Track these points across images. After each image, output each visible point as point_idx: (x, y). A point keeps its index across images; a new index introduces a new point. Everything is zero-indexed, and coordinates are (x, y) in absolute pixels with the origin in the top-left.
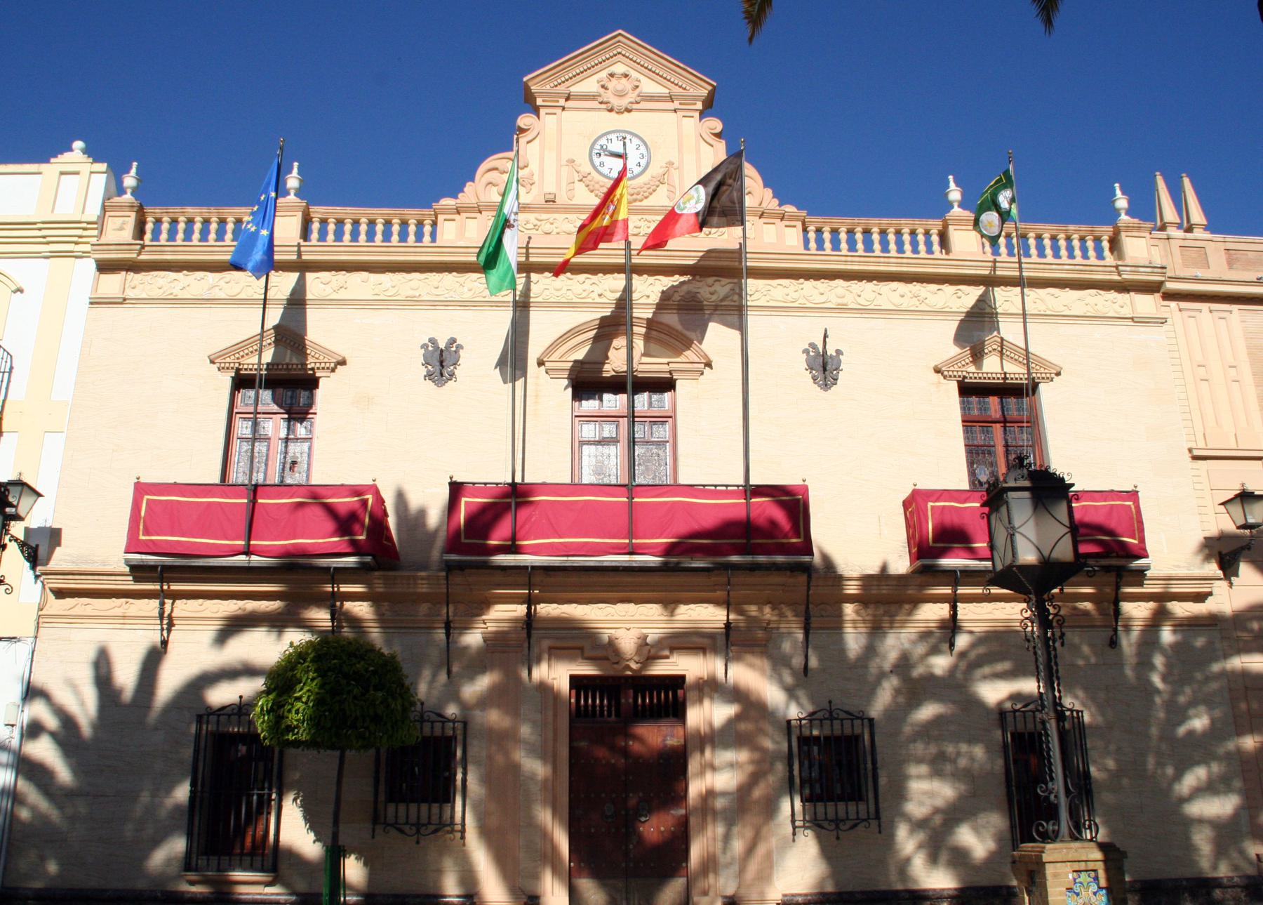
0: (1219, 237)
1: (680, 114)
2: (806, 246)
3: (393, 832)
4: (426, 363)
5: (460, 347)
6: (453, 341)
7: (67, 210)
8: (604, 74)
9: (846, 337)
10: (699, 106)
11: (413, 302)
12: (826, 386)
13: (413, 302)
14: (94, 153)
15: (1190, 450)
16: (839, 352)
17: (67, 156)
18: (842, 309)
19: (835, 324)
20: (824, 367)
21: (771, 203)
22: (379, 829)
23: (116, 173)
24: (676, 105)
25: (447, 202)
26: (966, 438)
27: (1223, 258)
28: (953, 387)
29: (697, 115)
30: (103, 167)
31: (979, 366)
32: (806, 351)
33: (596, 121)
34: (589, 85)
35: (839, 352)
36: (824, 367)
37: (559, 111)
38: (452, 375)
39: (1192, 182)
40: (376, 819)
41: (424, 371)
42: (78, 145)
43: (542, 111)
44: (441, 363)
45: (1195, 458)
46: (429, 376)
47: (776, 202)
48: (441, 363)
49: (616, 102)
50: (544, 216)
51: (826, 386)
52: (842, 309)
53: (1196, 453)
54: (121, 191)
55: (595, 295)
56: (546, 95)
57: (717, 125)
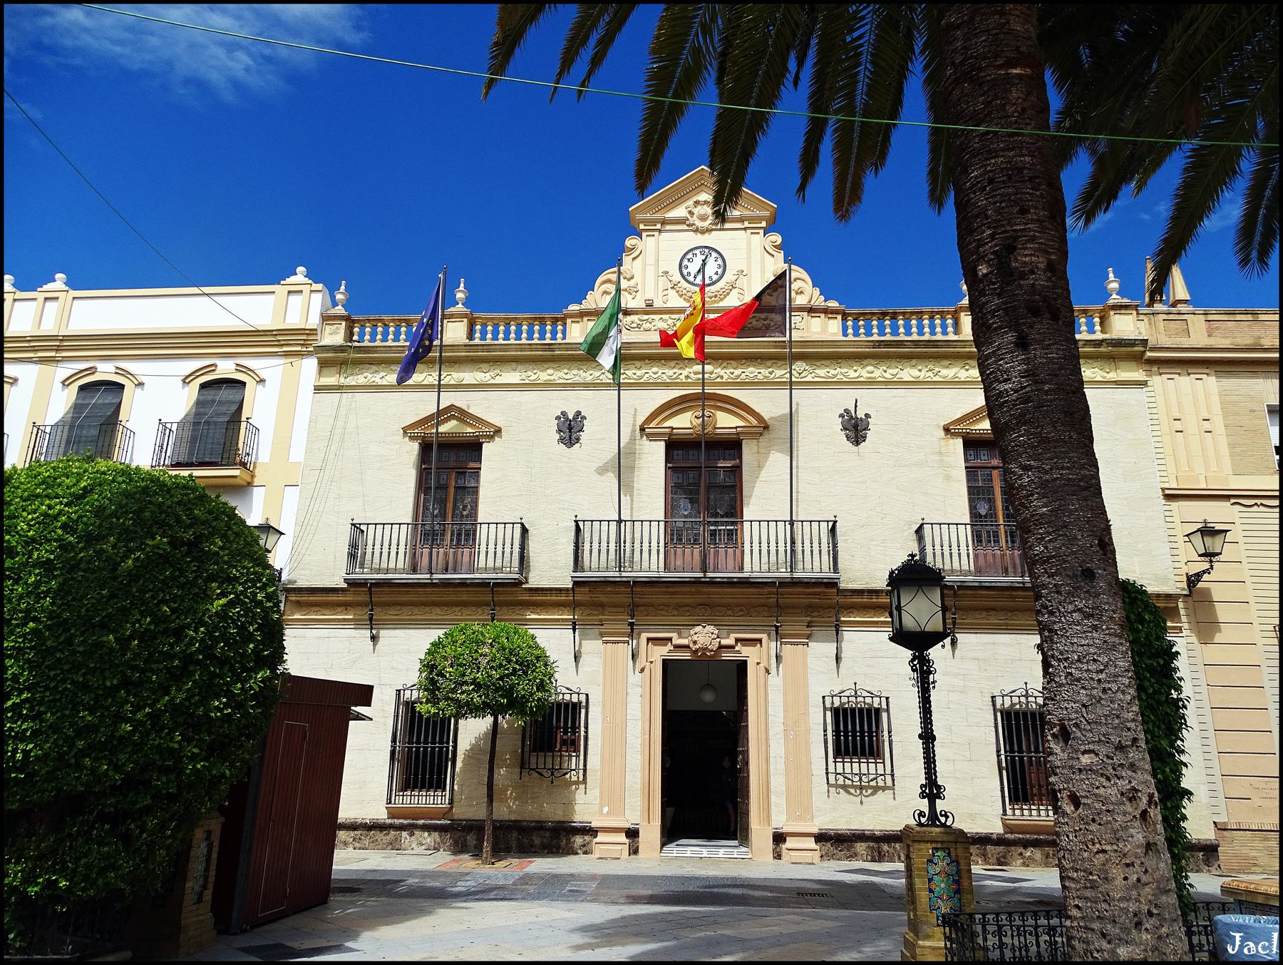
0: (1200, 310)
1: (749, 231)
2: (845, 335)
3: (535, 775)
4: (560, 431)
5: (584, 418)
6: (578, 413)
7: (294, 320)
8: (690, 202)
9: (869, 402)
10: (764, 224)
11: (548, 386)
12: (857, 443)
13: (548, 386)
14: (313, 276)
15: (1163, 489)
16: (867, 416)
17: (292, 279)
18: (871, 383)
19: (864, 395)
20: (856, 429)
21: (819, 301)
22: (525, 772)
23: (332, 289)
24: (746, 224)
25: (573, 308)
26: (968, 481)
27: (1203, 325)
28: (960, 441)
29: (762, 232)
30: (319, 286)
31: (779, 283)
32: (841, 416)
33: (679, 241)
34: (680, 212)
35: (867, 416)
36: (856, 429)
37: (656, 234)
38: (578, 440)
39: (1183, 273)
40: (523, 765)
41: (558, 437)
42: (301, 269)
43: (644, 234)
44: (570, 430)
45: (1169, 497)
46: (561, 440)
47: (822, 298)
48: (570, 430)
49: (699, 224)
50: (646, 317)
51: (857, 443)
52: (871, 383)
53: (1167, 492)
54: (335, 304)
55: (682, 377)
56: (646, 222)
57: (777, 238)
